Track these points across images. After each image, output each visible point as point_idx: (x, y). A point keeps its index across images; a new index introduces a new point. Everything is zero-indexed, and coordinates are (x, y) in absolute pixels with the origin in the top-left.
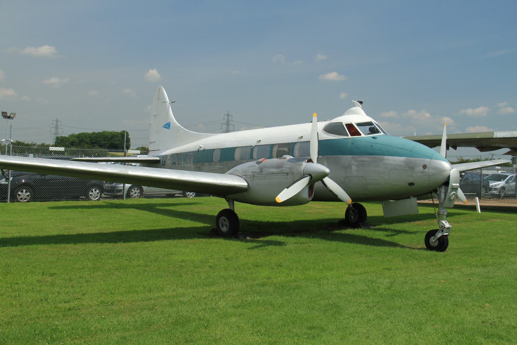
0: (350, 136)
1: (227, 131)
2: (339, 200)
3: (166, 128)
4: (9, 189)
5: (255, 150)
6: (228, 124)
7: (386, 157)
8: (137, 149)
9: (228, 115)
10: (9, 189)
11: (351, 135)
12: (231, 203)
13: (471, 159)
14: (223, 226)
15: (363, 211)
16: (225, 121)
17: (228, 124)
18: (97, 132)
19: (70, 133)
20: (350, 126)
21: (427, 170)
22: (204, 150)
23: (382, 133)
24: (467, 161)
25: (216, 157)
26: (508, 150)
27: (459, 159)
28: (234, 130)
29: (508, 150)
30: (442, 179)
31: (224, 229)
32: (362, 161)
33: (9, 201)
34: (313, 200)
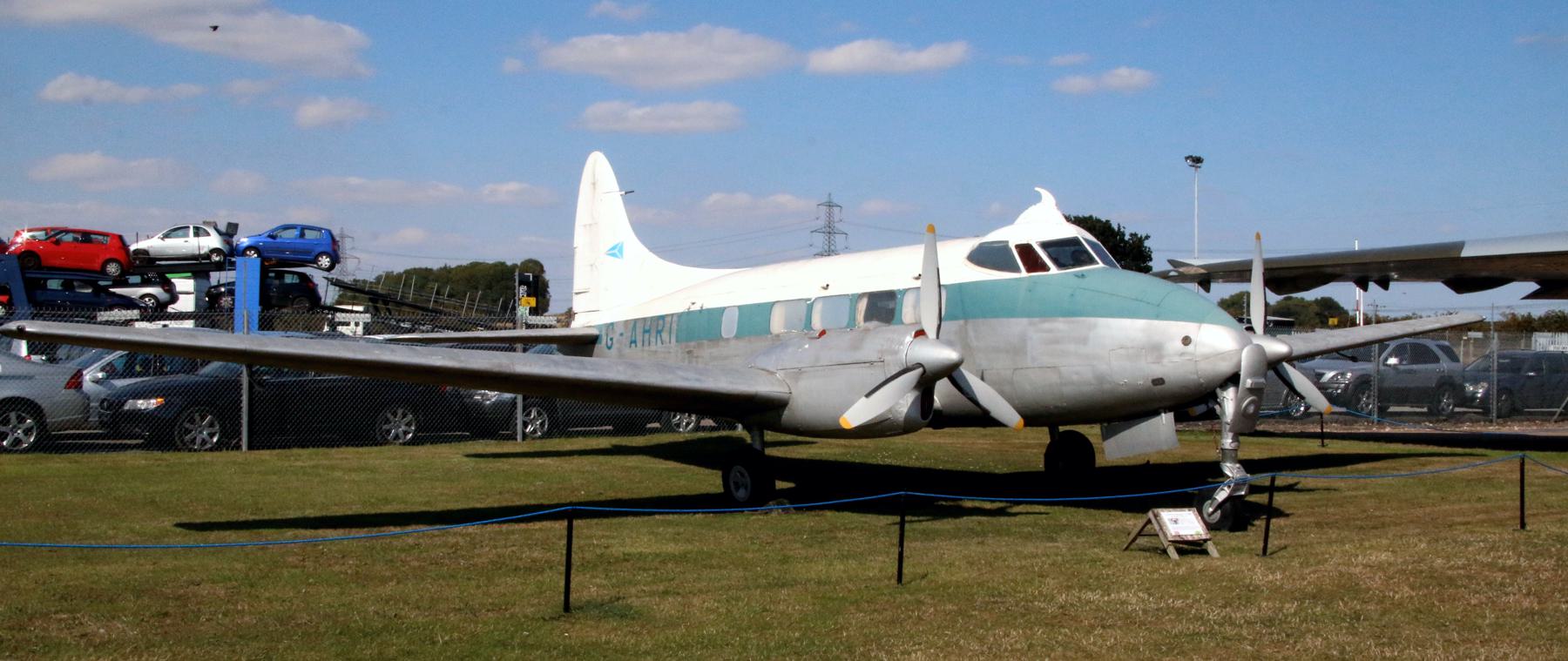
0: (1024, 273)
1: (829, 252)
2: (996, 423)
3: (614, 255)
4: (245, 398)
5: (817, 308)
6: (830, 231)
7: (1102, 321)
8: (343, 336)
9: (830, 205)
10: (245, 398)
11: (1029, 270)
12: (757, 433)
13: (1392, 316)
14: (737, 488)
15: (1084, 448)
16: (821, 223)
17: (830, 231)
18: (453, 264)
19: (381, 271)
20: (1026, 251)
21: (1190, 348)
22: (701, 311)
23: (1101, 265)
24: (1386, 320)
25: (729, 327)
26: (1533, 287)
27: (1503, 314)
28: (847, 249)
29: (1533, 287)
30: (1225, 368)
31: (741, 494)
32: (1050, 331)
33: (244, 447)
34: (928, 426)
